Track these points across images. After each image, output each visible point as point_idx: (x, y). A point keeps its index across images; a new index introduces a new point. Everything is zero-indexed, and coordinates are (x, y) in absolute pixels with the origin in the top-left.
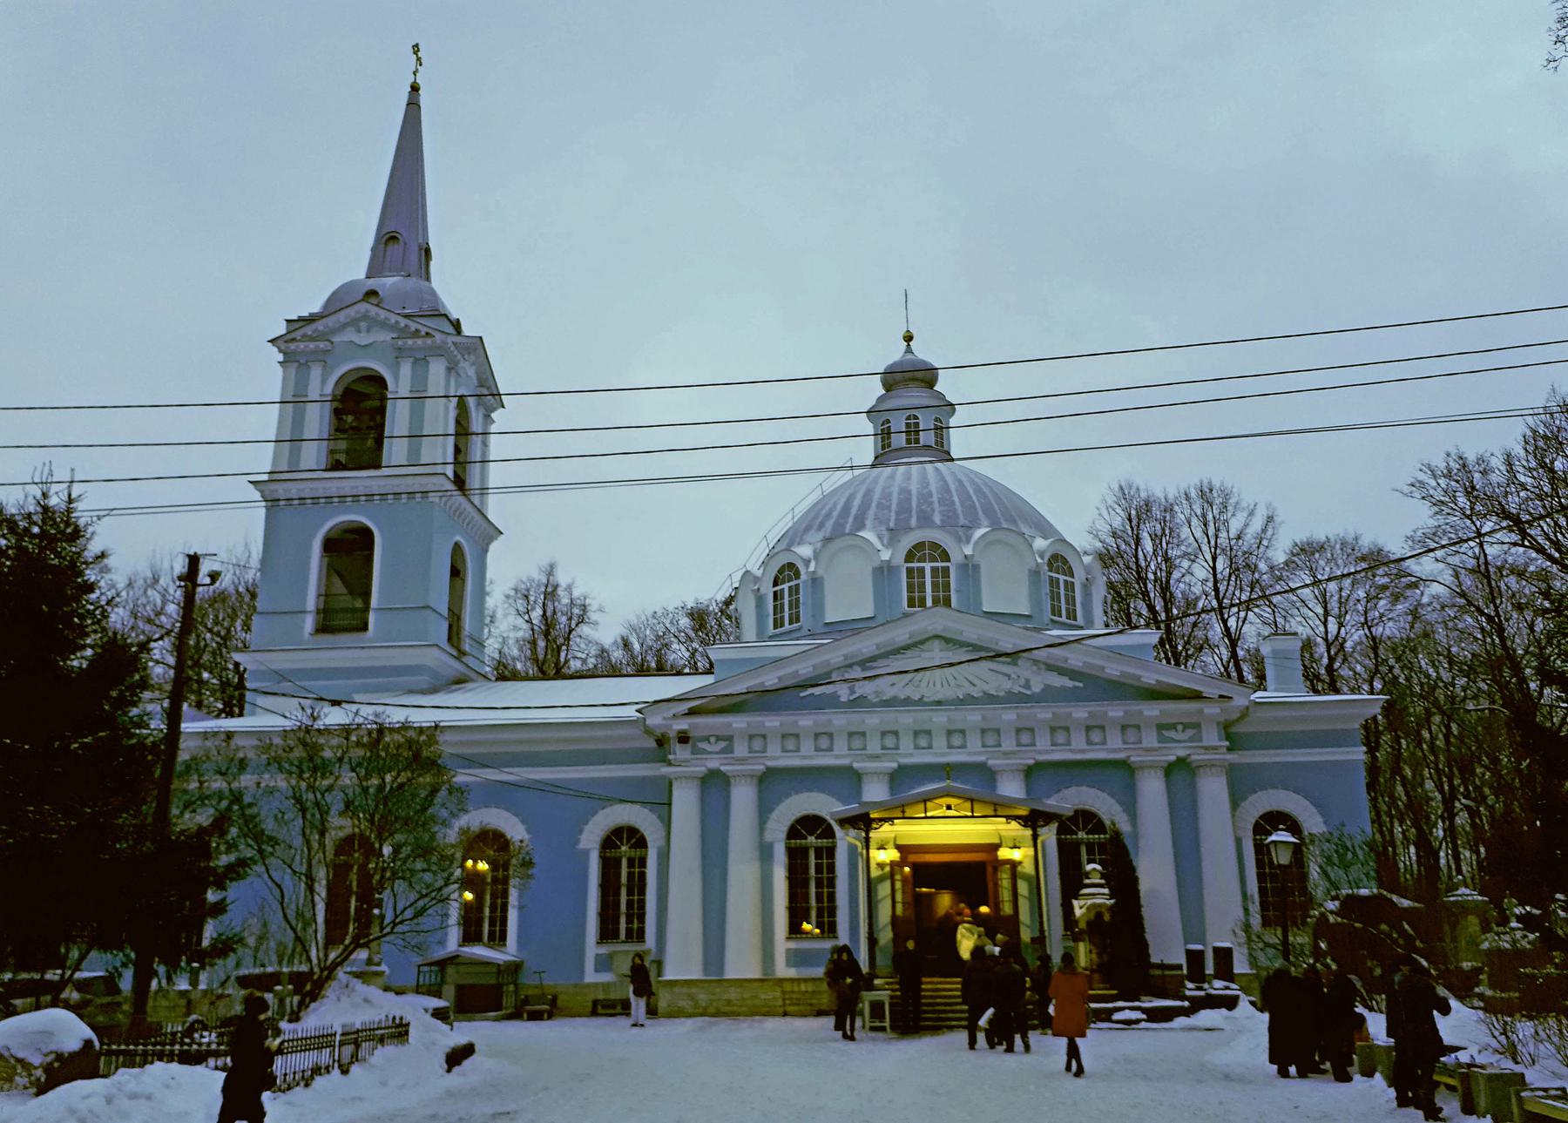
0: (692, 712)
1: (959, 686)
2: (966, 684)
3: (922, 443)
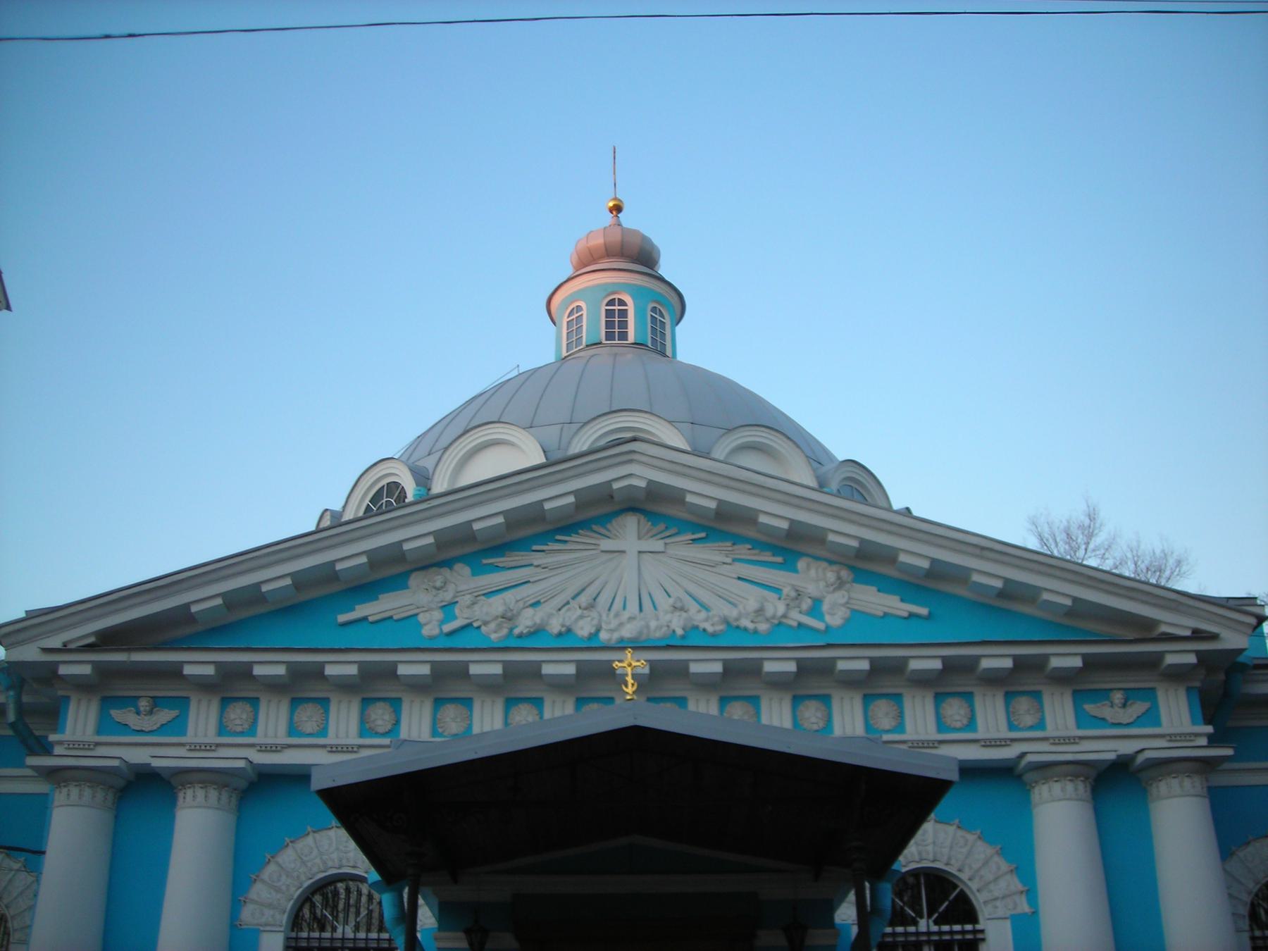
0: (107, 640)
1: (678, 608)
2: (693, 607)
3: (631, 338)
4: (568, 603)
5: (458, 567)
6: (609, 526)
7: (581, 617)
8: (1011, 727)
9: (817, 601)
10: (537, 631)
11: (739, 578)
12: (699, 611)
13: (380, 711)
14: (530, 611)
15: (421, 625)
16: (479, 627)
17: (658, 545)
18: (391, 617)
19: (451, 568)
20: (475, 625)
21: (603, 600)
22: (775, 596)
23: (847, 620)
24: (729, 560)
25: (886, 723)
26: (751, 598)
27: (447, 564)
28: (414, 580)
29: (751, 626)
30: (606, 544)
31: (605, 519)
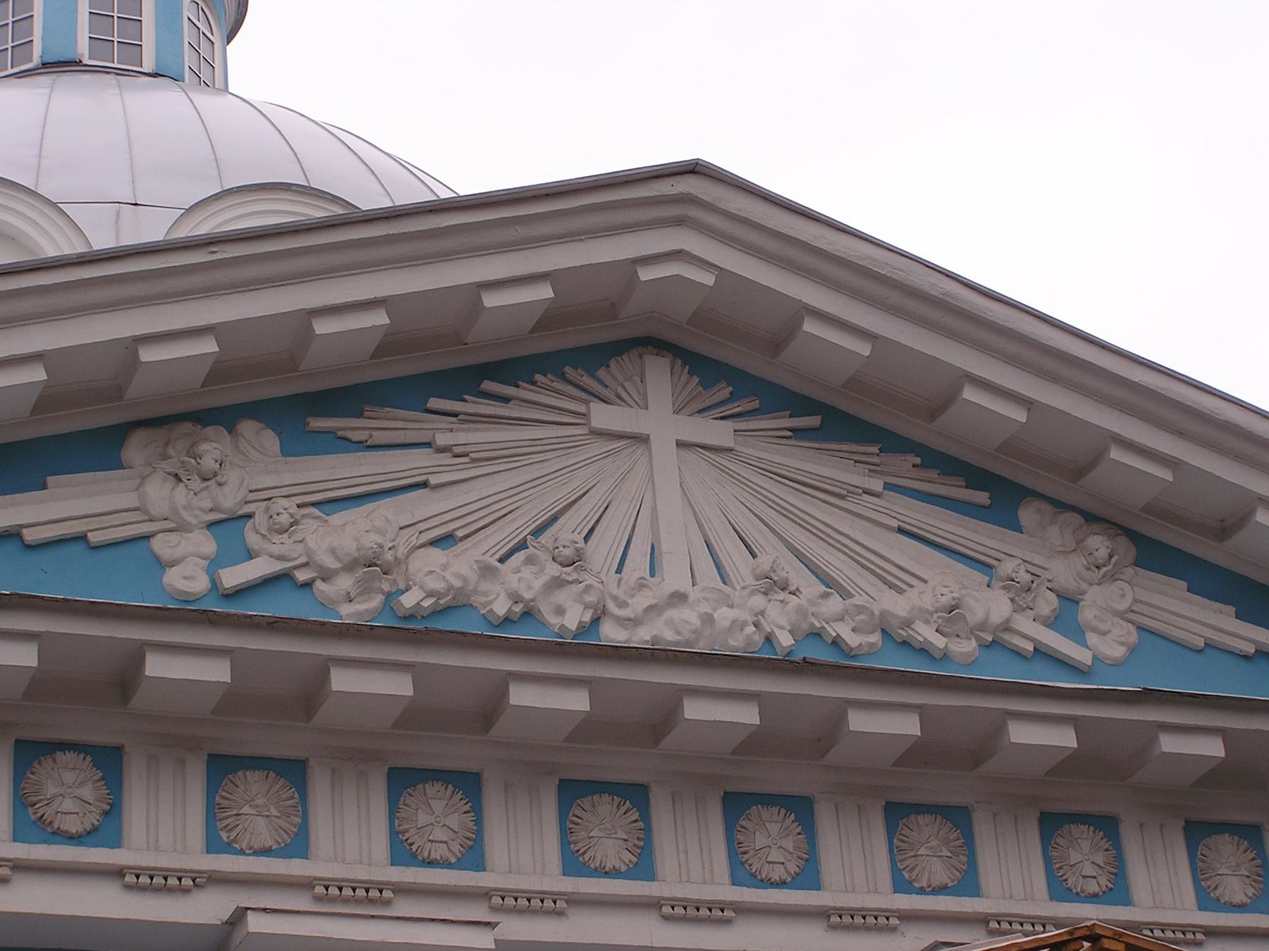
1: (773, 584)
2: (810, 587)
4: (522, 545)
5: (248, 427)
6: (601, 373)
7: (558, 583)
8: (214, 845)
9: (1069, 600)
10: (456, 604)
11: (900, 530)
12: (825, 596)
13: (69, 777)
14: (436, 556)
15: (163, 565)
16: (308, 585)
17: (719, 432)
18: (82, 538)
19: (231, 429)
20: (301, 576)
21: (602, 552)
22: (978, 577)
23: (1133, 650)
24: (876, 484)
25: (611, 851)
26: (941, 581)
27: (225, 418)
28: (136, 450)
29: (939, 641)
30: (603, 417)
31: (597, 356)
